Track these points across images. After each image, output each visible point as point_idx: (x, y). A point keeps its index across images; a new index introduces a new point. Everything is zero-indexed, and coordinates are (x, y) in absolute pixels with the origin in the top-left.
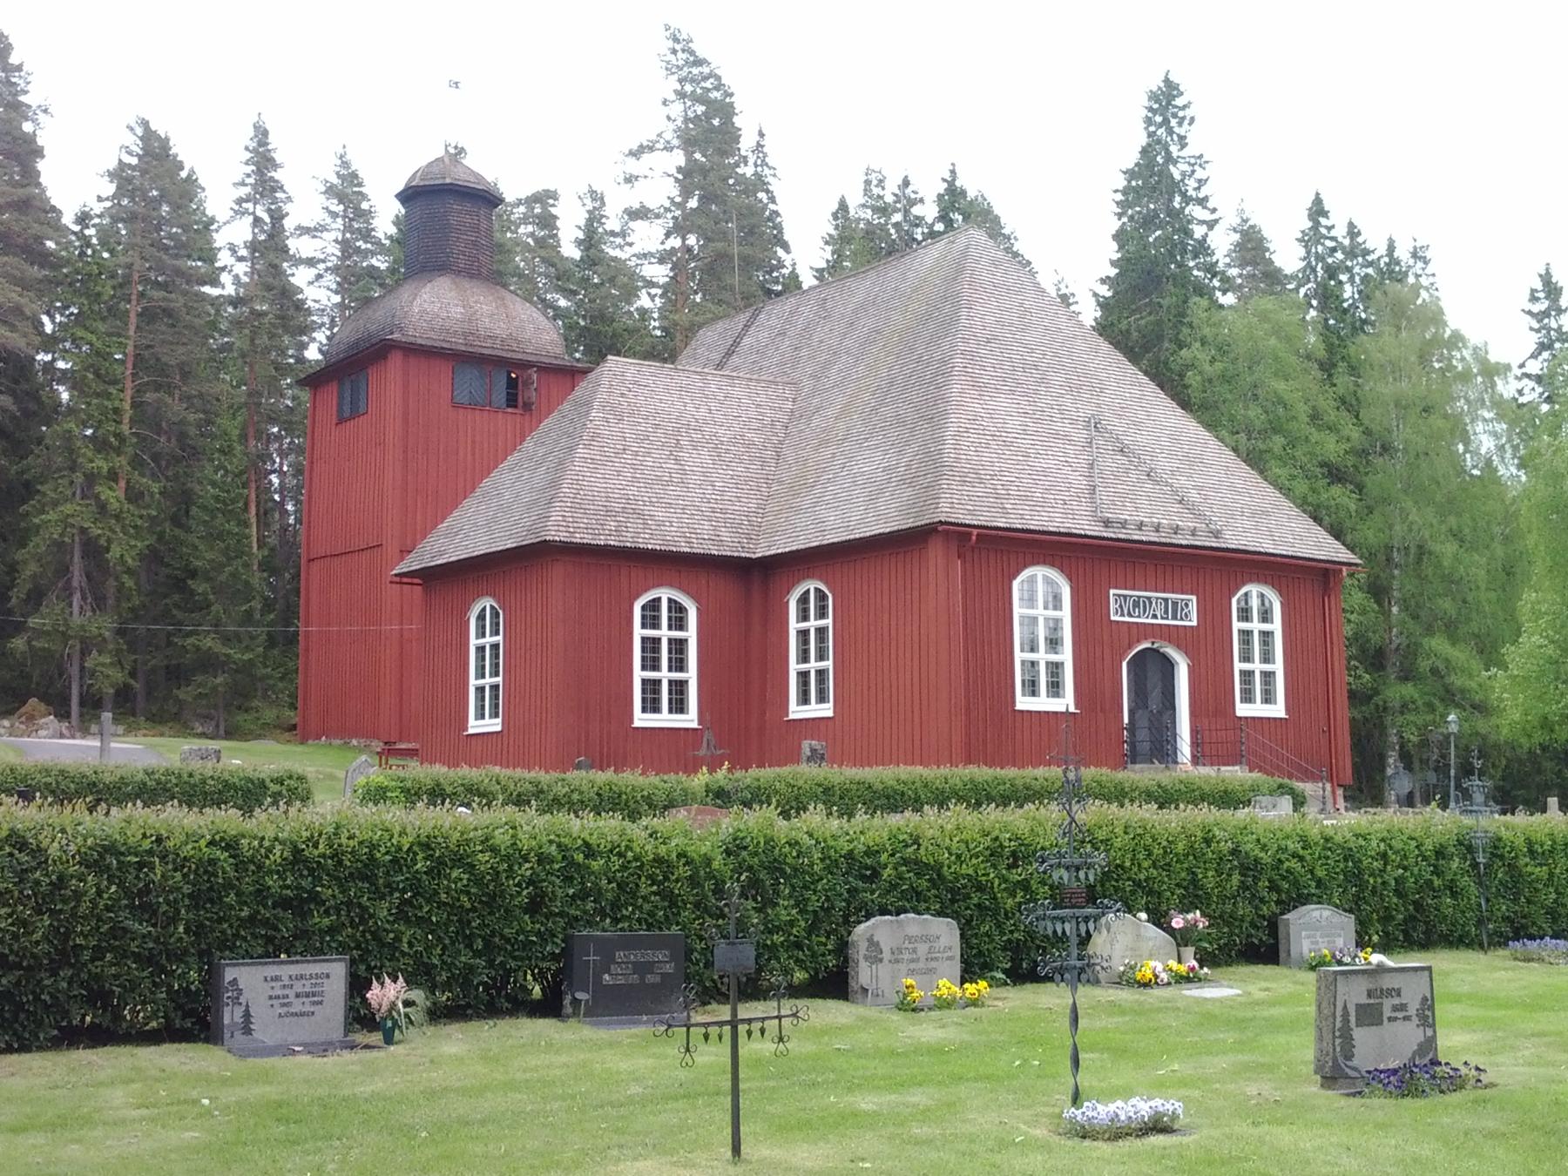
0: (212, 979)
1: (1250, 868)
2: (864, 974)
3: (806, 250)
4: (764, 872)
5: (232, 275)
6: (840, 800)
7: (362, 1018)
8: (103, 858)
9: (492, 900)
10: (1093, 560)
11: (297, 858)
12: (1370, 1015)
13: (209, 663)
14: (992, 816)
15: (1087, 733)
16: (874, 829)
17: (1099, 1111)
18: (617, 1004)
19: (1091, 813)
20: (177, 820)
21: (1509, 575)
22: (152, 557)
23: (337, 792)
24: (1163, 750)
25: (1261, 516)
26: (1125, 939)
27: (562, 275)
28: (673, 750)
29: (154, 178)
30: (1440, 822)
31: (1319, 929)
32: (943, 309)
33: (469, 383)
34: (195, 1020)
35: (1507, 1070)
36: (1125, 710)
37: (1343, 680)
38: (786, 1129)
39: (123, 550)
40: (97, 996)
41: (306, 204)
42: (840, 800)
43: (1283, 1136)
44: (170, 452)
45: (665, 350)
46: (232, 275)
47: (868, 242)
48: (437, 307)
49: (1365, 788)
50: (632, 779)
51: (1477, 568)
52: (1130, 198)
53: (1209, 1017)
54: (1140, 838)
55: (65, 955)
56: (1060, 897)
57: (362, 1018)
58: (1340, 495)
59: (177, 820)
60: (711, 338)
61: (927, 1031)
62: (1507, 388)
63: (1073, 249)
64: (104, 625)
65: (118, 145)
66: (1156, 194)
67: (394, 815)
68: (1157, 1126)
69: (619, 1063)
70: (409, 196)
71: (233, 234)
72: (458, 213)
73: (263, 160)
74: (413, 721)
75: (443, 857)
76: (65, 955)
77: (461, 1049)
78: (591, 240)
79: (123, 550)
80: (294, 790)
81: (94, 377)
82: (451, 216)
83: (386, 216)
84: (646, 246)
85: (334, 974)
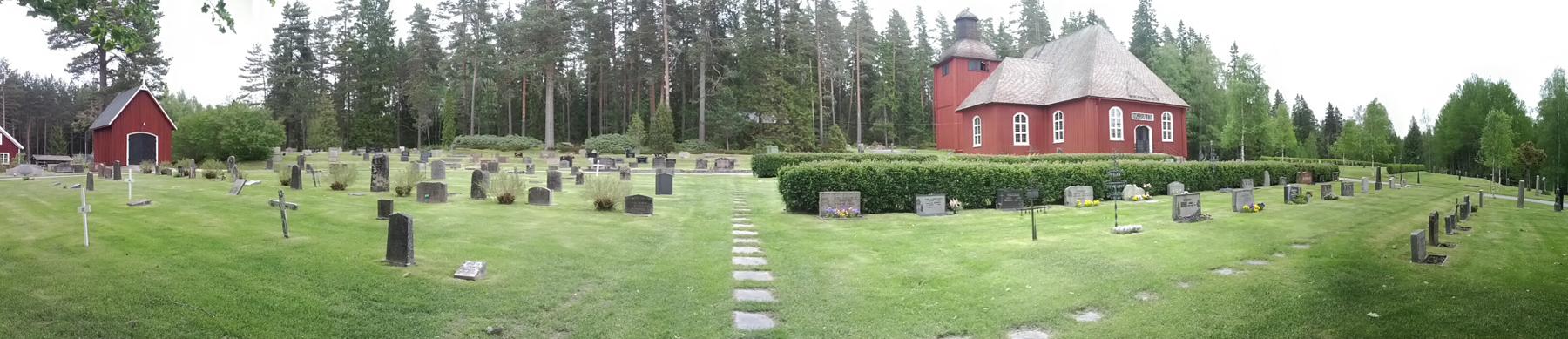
0: (914, 200)
1: (1161, 174)
2: (1068, 199)
3: (1056, 30)
4: (1044, 176)
5: (915, 43)
6: (1063, 160)
7: (949, 208)
8: (889, 172)
9: (977, 182)
10: (1128, 105)
11: (932, 172)
12: (1184, 205)
13: (914, 133)
14: (1101, 163)
15: (1126, 146)
16: (1070, 166)
17: (1121, 228)
18: (1007, 206)
19: (1121, 162)
20: (905, 164)
21: (1225, 112)
22: (901, 109)
23: (944, 159)
24: (1146, 149)
25: (1170, 97)
26: (1131, 190)
27: (995, 38)
28: (1024, 150)
29: (896, 22)
30: (1206, 164)
31: (1176, 187)
32: (1091, 42)
33: (972, 65)
34: (911, 208)
35: (1215, 216)
36: (1138, 138)
37: (1186, 134)
38: (1048, 233)
39: (894, 108)
40: (890, 202)
41: (931, 24)
42: (1063, 160)
43: (1164, 232)
44: (903, 85)
45: (1020, 55)
46: (915, 43)
47: (1070, 28)
48: (964, 47)
49: (1192, 154)
50: (1012, 156)
51: (1218, 109)
52: (1136, 18)
53: (1151, 207)
54: (1135, 168)
55: (882, 193)
56: (1114, 180)
57: (949, 208)
58: (1186, 91)
59: (905, 164)
60: (1031, 51)
61: (1082, 212)
62: (1225, 68)
63: (1124, 32)
64: (891, 125)
65: (888, 16)
66: (1143, 17)
67: (954, 163)
68: (1134, 231)
69: (1008, 219)
70: (957, 21)
71: (914, 33)
72: (968, 24)
73: (920, 14)
74: (961, 145)
75: (966, 173)
76: (882, 193)
77: (971, 215)
78: (1001, 30)
79: (894, 108)
80: (934, 158)
81: (887, 69)
82: (967, 25)
83: (951, 26)
84: (1014, 30)
85: (943, 197)
